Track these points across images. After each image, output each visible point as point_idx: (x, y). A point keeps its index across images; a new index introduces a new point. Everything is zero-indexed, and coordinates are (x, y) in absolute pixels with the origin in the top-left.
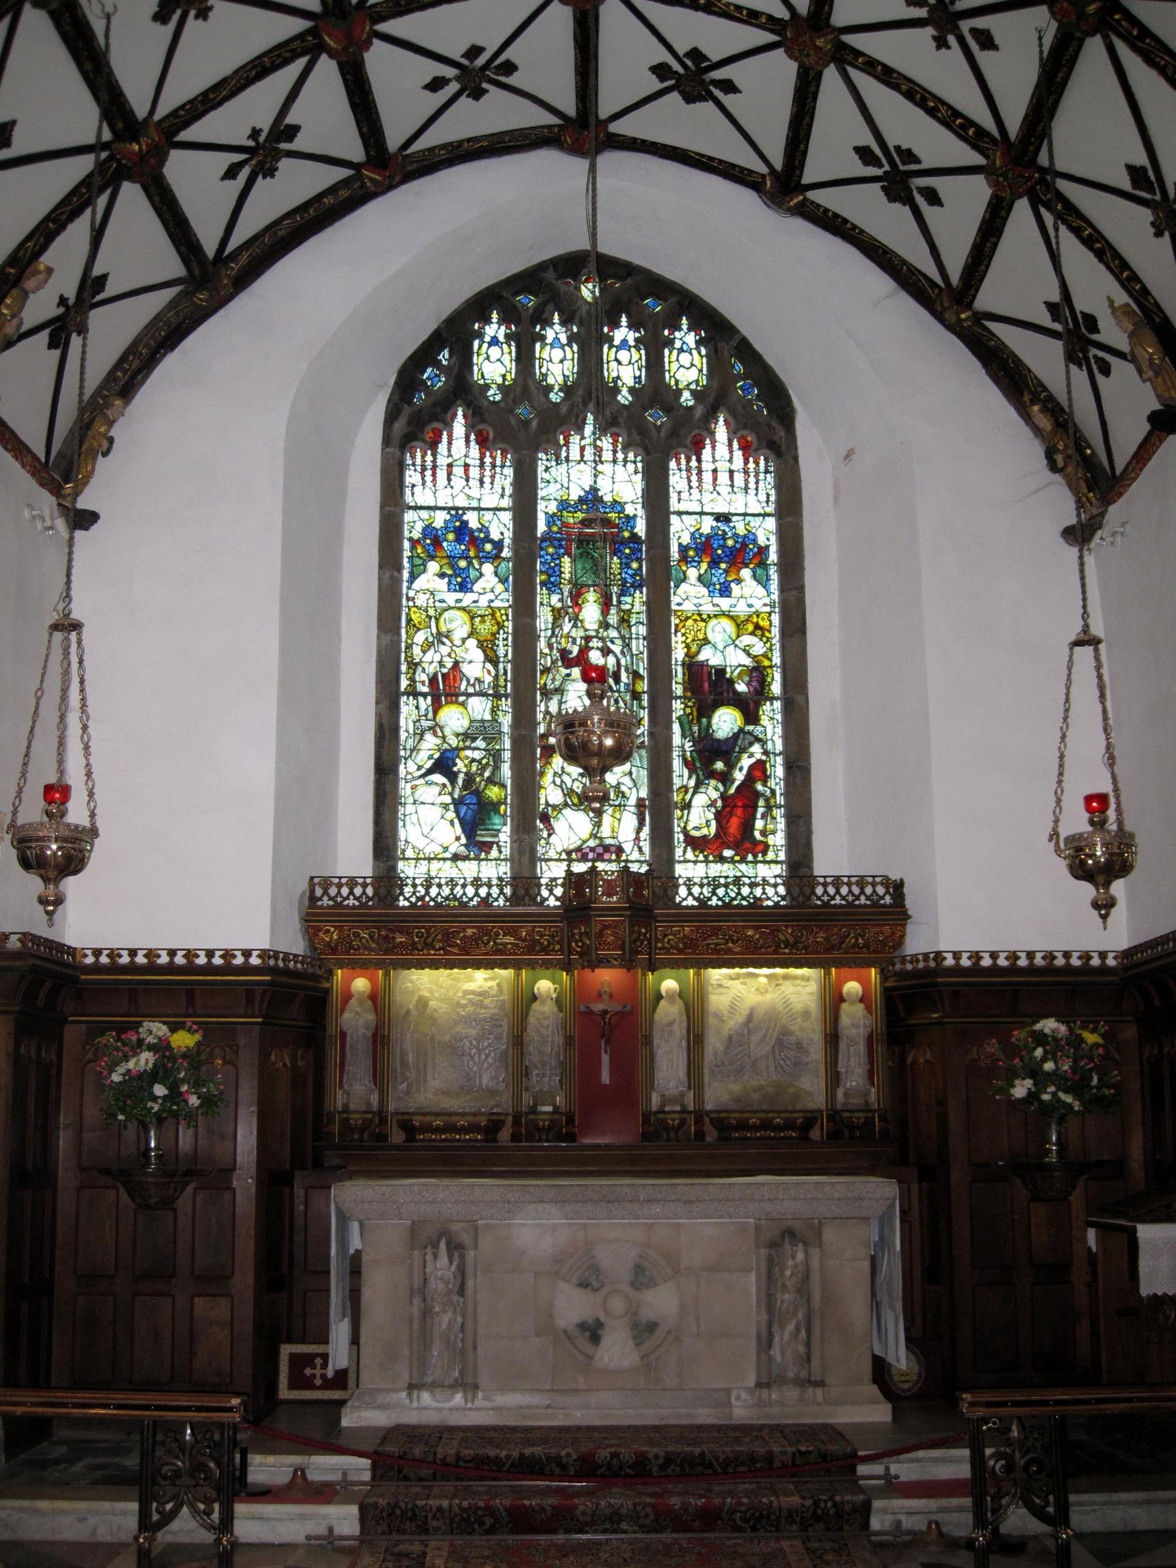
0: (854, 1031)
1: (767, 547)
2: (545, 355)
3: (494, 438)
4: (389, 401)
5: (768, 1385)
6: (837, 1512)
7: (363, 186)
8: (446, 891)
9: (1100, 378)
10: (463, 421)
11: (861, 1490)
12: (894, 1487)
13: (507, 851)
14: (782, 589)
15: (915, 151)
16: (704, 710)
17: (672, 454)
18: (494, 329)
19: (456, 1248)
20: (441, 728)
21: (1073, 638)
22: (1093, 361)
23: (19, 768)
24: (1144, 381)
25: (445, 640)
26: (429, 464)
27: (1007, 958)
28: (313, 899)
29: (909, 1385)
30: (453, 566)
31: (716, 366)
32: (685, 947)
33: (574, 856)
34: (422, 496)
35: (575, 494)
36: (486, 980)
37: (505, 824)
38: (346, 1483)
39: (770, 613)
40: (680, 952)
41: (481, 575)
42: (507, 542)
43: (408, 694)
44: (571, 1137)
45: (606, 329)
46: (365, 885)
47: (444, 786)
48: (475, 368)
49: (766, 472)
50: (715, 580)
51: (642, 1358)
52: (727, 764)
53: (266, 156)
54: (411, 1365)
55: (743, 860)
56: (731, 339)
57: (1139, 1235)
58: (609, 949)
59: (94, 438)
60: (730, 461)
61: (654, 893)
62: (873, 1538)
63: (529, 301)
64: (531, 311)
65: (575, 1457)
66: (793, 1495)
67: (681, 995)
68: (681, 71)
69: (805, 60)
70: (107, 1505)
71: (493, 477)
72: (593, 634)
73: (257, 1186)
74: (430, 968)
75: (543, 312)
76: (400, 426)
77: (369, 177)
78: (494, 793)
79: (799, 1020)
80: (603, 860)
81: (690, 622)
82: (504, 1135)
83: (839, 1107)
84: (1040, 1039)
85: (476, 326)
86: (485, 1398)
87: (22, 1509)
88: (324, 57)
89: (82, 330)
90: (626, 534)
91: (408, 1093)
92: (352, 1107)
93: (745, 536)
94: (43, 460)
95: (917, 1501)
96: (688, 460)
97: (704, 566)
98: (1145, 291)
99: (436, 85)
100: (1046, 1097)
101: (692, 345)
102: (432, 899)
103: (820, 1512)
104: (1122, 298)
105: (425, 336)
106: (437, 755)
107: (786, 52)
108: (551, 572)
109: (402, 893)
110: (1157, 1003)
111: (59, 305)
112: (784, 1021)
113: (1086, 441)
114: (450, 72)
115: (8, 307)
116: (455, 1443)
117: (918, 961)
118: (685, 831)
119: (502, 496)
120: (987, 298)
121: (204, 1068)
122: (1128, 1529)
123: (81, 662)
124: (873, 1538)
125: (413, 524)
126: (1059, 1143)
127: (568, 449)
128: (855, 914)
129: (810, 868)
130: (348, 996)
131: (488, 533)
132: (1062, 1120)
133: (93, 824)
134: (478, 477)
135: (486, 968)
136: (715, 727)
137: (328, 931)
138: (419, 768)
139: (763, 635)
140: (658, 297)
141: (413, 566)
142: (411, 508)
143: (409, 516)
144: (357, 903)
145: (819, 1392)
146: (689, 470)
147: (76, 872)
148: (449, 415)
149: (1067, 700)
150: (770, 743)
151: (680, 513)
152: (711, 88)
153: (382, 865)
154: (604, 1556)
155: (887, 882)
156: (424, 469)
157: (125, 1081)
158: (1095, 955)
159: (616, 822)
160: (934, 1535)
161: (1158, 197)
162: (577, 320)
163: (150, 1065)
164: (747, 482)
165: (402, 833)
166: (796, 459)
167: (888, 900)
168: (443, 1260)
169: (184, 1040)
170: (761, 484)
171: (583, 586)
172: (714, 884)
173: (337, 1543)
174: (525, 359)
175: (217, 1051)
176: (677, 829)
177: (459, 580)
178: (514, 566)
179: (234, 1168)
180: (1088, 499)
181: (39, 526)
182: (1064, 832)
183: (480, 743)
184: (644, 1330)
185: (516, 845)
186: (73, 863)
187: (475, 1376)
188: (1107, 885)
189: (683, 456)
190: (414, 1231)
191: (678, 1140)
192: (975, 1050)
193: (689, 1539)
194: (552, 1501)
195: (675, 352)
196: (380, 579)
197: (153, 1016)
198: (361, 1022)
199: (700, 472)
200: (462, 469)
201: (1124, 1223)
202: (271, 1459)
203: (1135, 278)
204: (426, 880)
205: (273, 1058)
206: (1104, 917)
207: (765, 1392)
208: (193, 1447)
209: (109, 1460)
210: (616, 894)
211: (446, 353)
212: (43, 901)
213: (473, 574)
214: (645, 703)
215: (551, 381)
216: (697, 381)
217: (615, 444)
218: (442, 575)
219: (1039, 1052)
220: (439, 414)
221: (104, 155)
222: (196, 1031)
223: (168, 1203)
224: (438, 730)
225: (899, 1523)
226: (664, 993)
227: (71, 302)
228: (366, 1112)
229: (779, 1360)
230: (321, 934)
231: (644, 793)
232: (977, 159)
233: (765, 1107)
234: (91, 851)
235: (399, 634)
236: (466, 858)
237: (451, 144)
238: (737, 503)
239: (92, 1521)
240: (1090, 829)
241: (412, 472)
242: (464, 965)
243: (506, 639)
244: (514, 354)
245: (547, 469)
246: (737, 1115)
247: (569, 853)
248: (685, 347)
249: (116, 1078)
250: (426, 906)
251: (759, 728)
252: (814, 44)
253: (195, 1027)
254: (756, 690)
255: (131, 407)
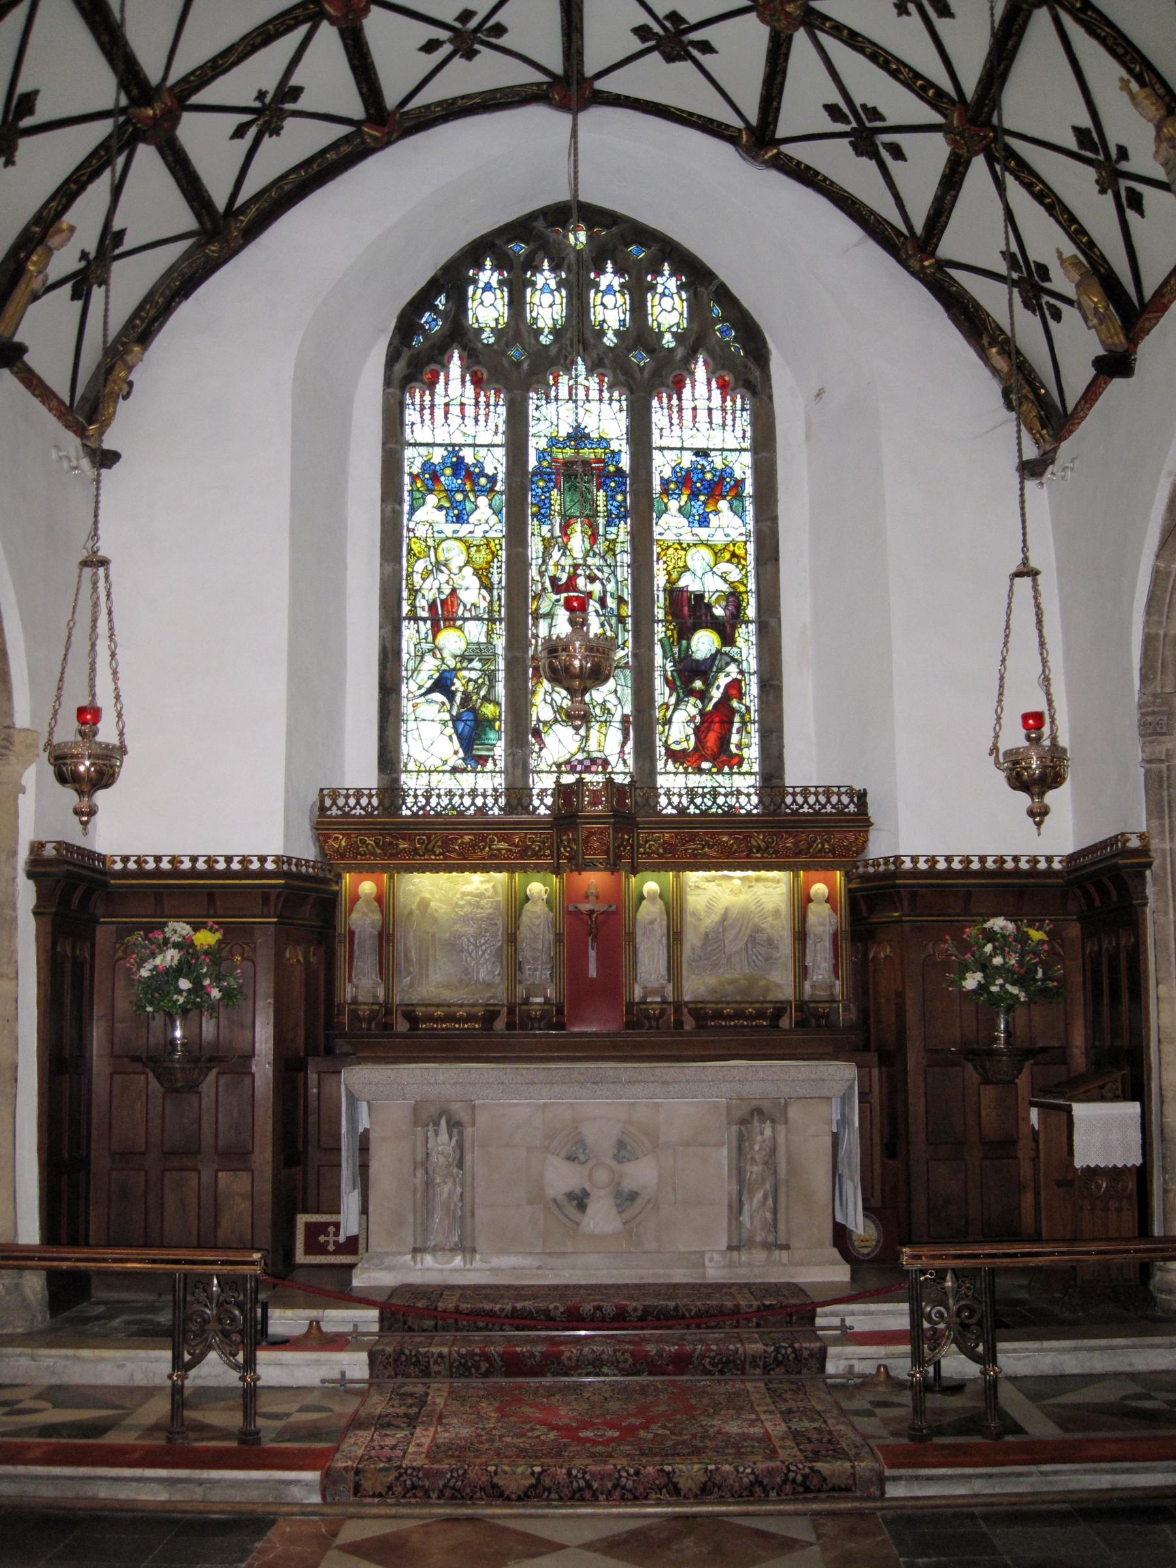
0: (821, 929)
1: (743, 480)
2: (536, 300)
3: (488, 379)
4: (390, 344)
5: (738, 1248)
6: (796, 1358)
7: (363, 142)
8: (445, 801)
9: (1052, 323)
10: (459, 363)
11: (818, 1338)
12: (849, 1336)
13: (501, 764)
14: (757, 520)
15: (881, 109)
16: (685, 632)
17: (654, 393)
18: (488, 275)
19: (455, 1125)
20: (440, 650)
21: (1013, 569)
22: (1045, 307)
23: (55, 693)
24: (1089, 328)
25: (443, 568)
26: (427, 403)
27: (961, 862)
28: (323, 809)
29: (869, 1250)
30: (450, 499)
31: (696, 309)
32: (665, 852)
33: (563, 768)
34: (421, 434)
35: (564, 430)
36: (482, 882)
37: (500, 739)
38: (356, 1333)
39: (745, 543)
40: (661, 856)
41: (477, 507)
42: (501, 476)
43: (410, 619)
44: (561, 1026)
45: (592, 275)
46: (370, 796)
47: (443, 704)
48: (470, 313)
49: (743, 409)
50: (694, 511)
51: (625, 1223)
52: (704, 683)
53: (272, 117)
54: (415, 1231)
55: (720, 772)
56: (710, 284)
57: (1074, 1113)
58: (595, 854)
59: (115, 382)
60: (709, 399)
61: (636, 802)
62: (829, 1381)
63: (520, 249)
64: (522, 259)
65: (562, 1310)
66: (756, 1342)
67: (661, 896)
68: (661, 32)
69: (776, 24)
70: (142, 1353)
71: (487, 415)
72: (580, 562)
73: (274, 1071)
74: (431, 871)
75: (533, 260)
76: (400, 367)
77: (368, 134)
78: (489, 710)
79: (770, 919)
80: (591, 772)
81: (671, 551)
82: (500, 1024)
83: (806, 998)
84: (990, 936)
85: (471, 273)
86: (482, 1261)
87: (67, 1357)
88: (325, 26)
89: (104, 282)
90: (612, 469)
91: (411, 985)
92: (361, 999)
93: (722, 470)
94: (68, 403)
95: (867, 1348)
96: (670, 399)
97: (684, 498)
98: (1091, 244)
99: (430, 47)
100: (994, 989)
101: (674, 290)
102: (432, 809)
103: (780, 1357)
104: (1070, 249)
105: (422, 283)
106: (436, 676)
107: (758, 16)
108: (541, 504)
109: (404, 803)
110: (1098, 903)
111: (80, 259)
112: (756, 920)
113: (1041, 382)
114: (444, 35)
115: (34, 264)
116: (455, 1299)
117: (879, 865)
118: (666, 746)
119: (496, 433)
120: (948, 248)
121: (224, 964)
122: (1058, 1373)
123: (109, 595)
124: (829, 1381)
125: (413, 460)
126: (1006, 1031)
127: (557, 389)
128: (820, 821)
129: (782, 778)
130: (355, 898)
131: (482, 468)
132: (1009, 1009)
133: (122, 742)
134: (473, 415)
135: (482, 872)
136: (694, 648)
137: (337, 838)
138: (420, 687)
139: (739, 563)
140: (641, 244)
141: (413, 499)
142: (411, 445)
143: (409, 452)
144: (363, 813)
145: (784, 1254)
146: (670, 408)
147: (107, 786)
148: (446, 357)
149: (1008, 627)
150: (745, 663)
151: (661, 449)
152: (690, 49)
153: (387, 777)
154: (586, 1395)
155: (851, 792)
156: (422, 408)
157: (153, 976)
158: (1042, 859)
159: (603, 737)
160: (882, 1378)
161: (1101, 158)
162: (565, 266)
163: (176, 962)
164: (724, 418)
165: (404, 748)
166: (770, 398)
167: (852, 808)
168: (444, 1136)
169: (206, 939)
170: (738, 421)
171: (571, 517)
172: (691, 793)
173: (349, 1385)
174: (516, 303)
175: (236, 949)
176: (658, 743)
177: (456, 512)
178: (508, 500)
179: (253, 1055)
180: (1042, 436)
181: (66, 465)
182: (1003, 748)
183: (476, 664)
184: (626, 1199)
185: (510, 759)
186: (104, 777)
187: (473, 1240)
188: (1041, 795)
189: (664, 395)
190: (416, 1109)
191: (658, 1028)
192: (930, 945)
193: (663, 1382)
194: (539, 1349)
195: (657, 296)
196: (383, 511)
197: (178, 916)
198: (368, 921)
199: (680, 410)
200: (458, 408)
201: (1062, 1102)
202: (289, 1313)
203: (1082, 231)
204: (427, 791)
205: (287, 955)
206: (1038, 824)
207: (735, 1254)
208: (219, 1296)
209: (142, 1316)
210: (601, 803)
211: (443, 298)
212: (78, 812)
213: (469, 506)
214: (629, 626)
215: (541, 324)
216: (678, 324)
217: (601, 383)
218: (440, 508)
219: (989, 948)
220: (436, 356)
221: (121, 119)
222: (217, 930)
223: (193, 1087)
224: (437, 652)
225: (851, 1367)
226: (645, 895)
227: (92, 256)
228: (373, 1004)
229: (748, 1225)
230: (330, 841)
231: (628, 710)
232: (936, 118)
233: (738, 998)
234: (120, 767)
235: (400, 563)
236: (464, 771)
237: (446, 101)
238: (713, 439)
239: (130, 1366)
240: (1027, 744)
241: (411, 411)
242: (461, 869)
243: (500, 567)
244: (506, 299)
245: (537, 408)
246: (714, 1006)
247: (559, 766)
248: (667, 292)
249: (145, 973)
250: (426, 815)
251: (735, 650)
252: (783, 9)
253: (216, 927)
254: (732, 613)
255: (148, 353)
